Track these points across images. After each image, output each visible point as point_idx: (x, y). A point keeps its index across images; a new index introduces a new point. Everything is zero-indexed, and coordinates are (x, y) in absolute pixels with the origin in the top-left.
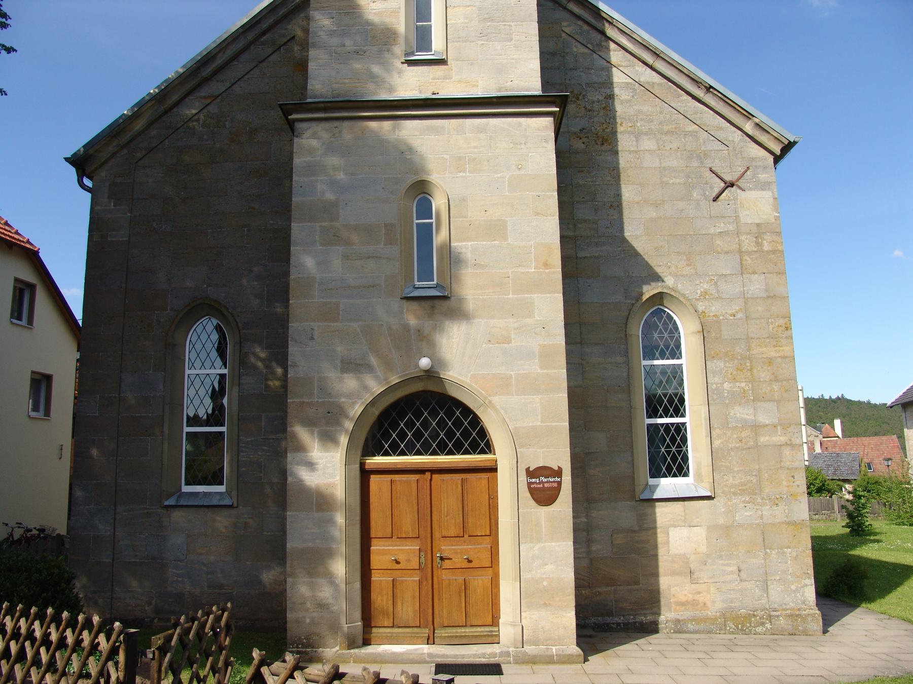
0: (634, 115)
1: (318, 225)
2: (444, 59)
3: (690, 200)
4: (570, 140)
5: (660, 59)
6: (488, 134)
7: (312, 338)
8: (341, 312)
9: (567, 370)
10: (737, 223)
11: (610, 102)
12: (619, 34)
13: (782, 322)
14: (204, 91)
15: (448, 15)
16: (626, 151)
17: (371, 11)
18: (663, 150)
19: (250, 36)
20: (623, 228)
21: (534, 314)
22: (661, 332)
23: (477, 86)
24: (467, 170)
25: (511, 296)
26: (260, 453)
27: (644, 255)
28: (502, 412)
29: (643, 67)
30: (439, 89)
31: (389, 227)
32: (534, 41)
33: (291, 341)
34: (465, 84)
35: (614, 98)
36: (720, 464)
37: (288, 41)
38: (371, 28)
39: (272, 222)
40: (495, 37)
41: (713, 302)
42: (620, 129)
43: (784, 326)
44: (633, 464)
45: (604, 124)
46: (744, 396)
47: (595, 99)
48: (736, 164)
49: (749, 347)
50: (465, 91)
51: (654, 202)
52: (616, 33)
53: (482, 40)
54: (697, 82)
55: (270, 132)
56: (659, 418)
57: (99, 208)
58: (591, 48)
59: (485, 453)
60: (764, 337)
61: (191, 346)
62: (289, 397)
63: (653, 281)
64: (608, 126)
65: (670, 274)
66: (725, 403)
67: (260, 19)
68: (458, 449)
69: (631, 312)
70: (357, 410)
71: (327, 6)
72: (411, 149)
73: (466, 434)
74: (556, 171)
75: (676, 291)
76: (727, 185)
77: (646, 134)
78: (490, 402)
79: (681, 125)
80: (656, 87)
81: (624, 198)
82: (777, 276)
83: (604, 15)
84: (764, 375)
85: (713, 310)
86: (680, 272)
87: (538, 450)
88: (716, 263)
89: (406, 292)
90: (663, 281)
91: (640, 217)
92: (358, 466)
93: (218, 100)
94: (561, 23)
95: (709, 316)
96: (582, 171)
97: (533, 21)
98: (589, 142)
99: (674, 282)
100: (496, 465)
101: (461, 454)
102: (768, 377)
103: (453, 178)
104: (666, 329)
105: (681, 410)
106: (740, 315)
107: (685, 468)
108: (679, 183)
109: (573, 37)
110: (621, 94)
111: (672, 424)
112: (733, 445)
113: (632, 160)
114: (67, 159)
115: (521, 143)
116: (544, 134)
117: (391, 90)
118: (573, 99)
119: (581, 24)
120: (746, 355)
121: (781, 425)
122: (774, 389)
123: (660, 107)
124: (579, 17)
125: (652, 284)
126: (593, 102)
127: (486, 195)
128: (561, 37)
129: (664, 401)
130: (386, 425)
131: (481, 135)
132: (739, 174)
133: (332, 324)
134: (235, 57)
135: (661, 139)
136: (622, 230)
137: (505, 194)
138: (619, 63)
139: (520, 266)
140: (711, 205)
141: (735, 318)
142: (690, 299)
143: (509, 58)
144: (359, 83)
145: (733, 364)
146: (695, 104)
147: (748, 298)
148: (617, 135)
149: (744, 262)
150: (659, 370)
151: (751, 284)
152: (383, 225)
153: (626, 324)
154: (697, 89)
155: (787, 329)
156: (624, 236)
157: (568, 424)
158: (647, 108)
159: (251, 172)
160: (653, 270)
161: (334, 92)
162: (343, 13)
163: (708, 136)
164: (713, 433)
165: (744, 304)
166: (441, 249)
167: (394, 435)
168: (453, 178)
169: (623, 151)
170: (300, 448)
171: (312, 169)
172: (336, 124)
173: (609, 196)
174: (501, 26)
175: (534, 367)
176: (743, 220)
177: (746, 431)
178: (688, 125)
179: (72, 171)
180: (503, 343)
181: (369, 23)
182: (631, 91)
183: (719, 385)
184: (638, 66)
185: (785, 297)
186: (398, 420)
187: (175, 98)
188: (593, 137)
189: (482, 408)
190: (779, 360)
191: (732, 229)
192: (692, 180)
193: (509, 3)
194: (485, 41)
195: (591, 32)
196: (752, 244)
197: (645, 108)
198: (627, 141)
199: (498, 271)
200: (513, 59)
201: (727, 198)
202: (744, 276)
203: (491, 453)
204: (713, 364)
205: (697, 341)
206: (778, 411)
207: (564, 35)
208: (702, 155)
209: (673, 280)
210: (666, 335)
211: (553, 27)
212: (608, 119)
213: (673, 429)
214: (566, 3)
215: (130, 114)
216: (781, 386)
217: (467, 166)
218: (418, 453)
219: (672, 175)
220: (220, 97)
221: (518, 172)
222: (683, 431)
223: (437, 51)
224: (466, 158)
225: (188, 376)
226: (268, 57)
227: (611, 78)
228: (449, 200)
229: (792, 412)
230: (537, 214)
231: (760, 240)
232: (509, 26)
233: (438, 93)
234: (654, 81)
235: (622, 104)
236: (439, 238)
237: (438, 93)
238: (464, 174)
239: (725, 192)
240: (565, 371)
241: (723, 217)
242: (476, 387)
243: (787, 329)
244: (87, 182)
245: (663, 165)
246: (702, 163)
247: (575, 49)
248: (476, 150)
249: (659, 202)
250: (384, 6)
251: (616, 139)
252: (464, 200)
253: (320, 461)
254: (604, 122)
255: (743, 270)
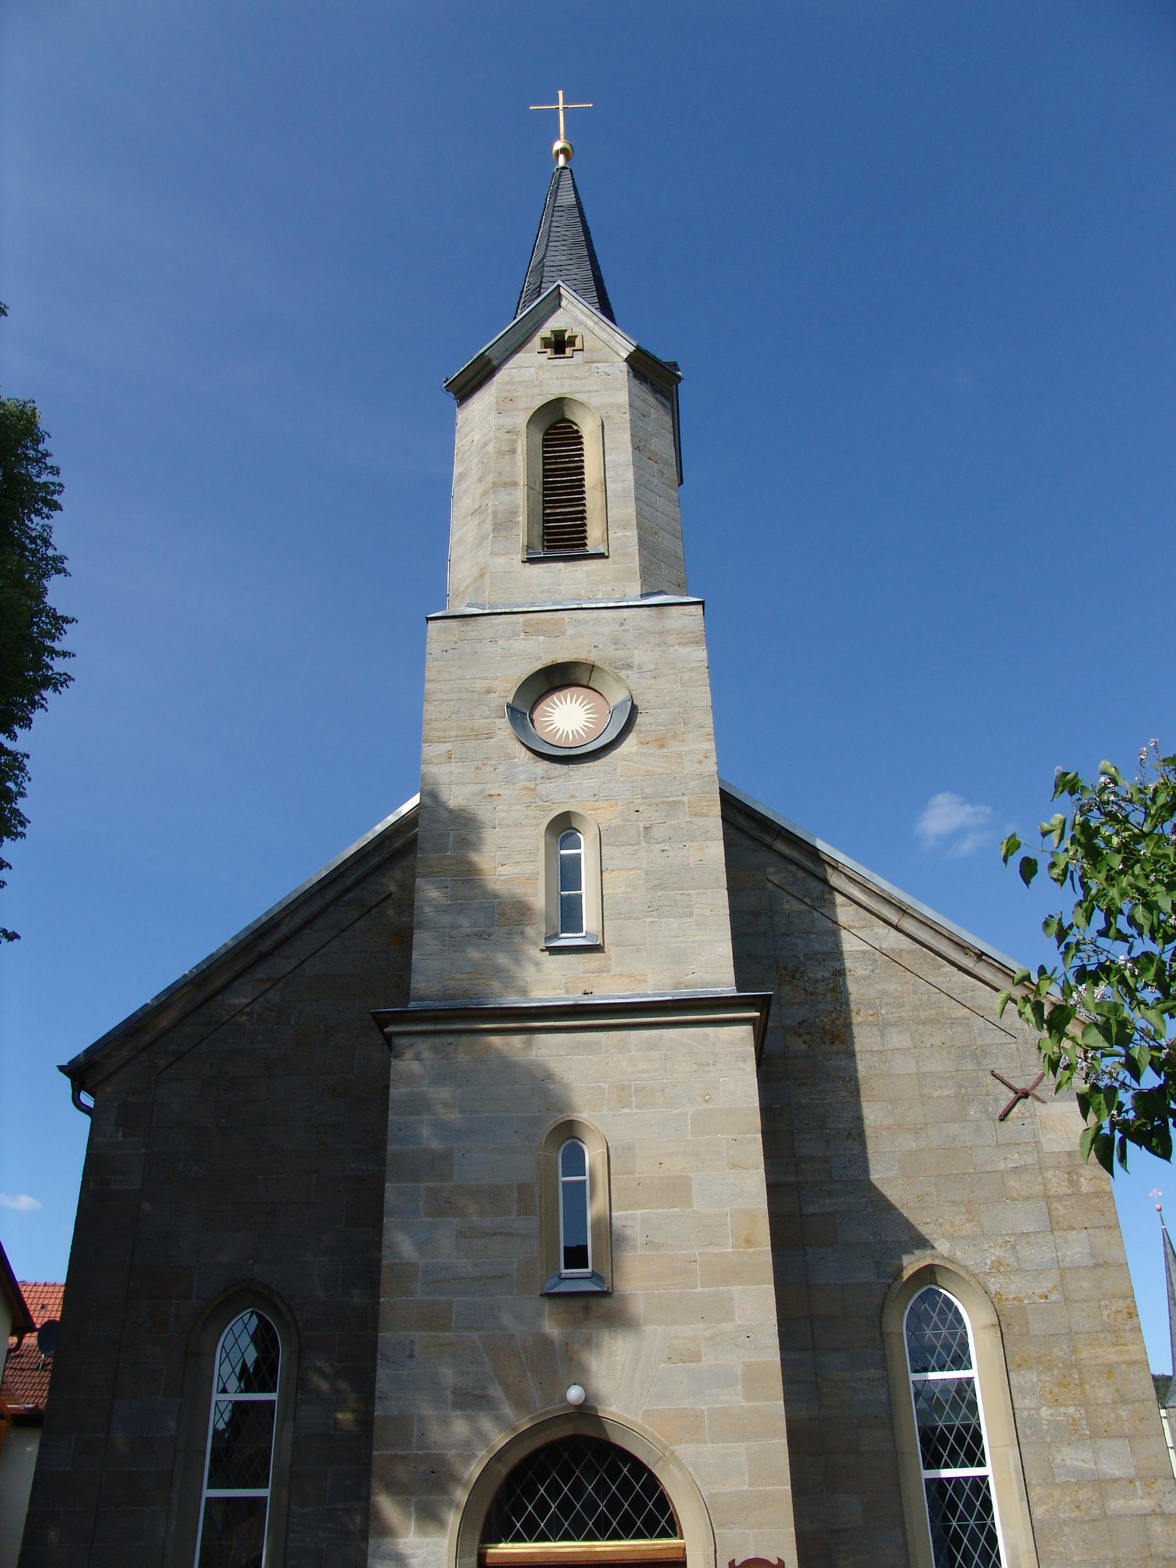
0: (877, 998)
1: (423, 1185)
2: (600, 944)
3: (966, 1120)
4: (784, 1038)
5: (908, 916)
6: (662, 1052)
7: (411, 1356)
8: (454, 1316)
9: (784, 1401)
10: (1038, 1153)
11: (841, 980)
12: (848, 882)
13: (1121, 1304)
14: (262, 972)
15: (603, 882)
16: (867, 1051)
17: (498, 877)
18: (921, 1048)
19: (330, 894)
20: (868, 1167)
21: (734, 1315)
22: (936, 1327)
23: (646, 982)
24: (634, 1104)
25: (699, 1289)
26: (321, 1534)
27: (902, 1208)
28: (691, 1469)
29: (885, 928)
30: (593, 987)
31: (524, 1190)
32: (723, 916)
33: (381, 1359)
34: (629, 978)
35: (845, 974)
36: (1048, 1548)
37: (382, 901)
38: (499, 902)
39: (353, 1166)
40: (670, 910)
41: (1011, 1277)
42: (856, 1019)
43: (1125, 1312)
44: (907, 1550)
45: (833, 1012)
46: (1075, 1430)
47: (819, 976)
48: (1029, 1063)
49: (1073, 1348)
50: (628, 989)
51: (912, 1126)
52: (844, 881)
53: (650, 916)
54: (963, 947)
55: (354, 1031)
56: (943, 1468)
57: (100, 1139)
58: (810, 904)
59: (668, 1536)
60: (1096, 1329)
61: (224, 1355)
62: (375, 1447)
63: (918, 1248)
64: (840, 1016)
65: (943, 1235)
66: (1046, 1442)
67: (344, 871)
68: (627, 1530)
69: (888, 1296)
70: (474, 1471)
71: (440, 870)
72: (549, 1076)
73: (638, 1505)
74: (758, 1103)
75: (954, 1263)
76: (1019, 1095)
77: (895, 1025)
78: (672, 1453)
79: (945, 1009)
80: (905, 956)
81: (866, 1122)
82: (1106, 1231)
83: (825, 858)
84: (1102, 1393)
85: (1012, 1290)
86: (958, 1232)
87: (746, 1531)
88: (1012, 1215)
89: (548, 1285)
90: (933, 1247)
91: (893, 1149)
92: (474, 1559)
93: (281, 984)
94: (765, 870)
95: (1007, 1300)
96: (804, 1084)
97: (720, 888)
98: (812, 1040)
99: (950, 1248)
100: (685, 1556)
101: (631, 1538)
102: (1109, 1397)
103: (614, 1116)
104: (944, 1321)
105: (977, 1454)
106: (1054, 1297)
107: (994, 1556)
108: (947, 1096)
109: (783, 889)
110: (855, 969)
111: (966, 1479)
112: (1067, 1515)
113: (877, 1064)
114: (61, 1068)
115: (708, 1064)
116: (739, 1049)
117: (524, 992)
118: (787, 978)
119: (794, 869)
120: (1072, 1362)
121: (1141, 1479)
122: (1121, 1416)
123: (913, 984)
124: (790, 861)
125: (916, 1252)
126: (816, 981)
127: (661, 1140)
128: (766, 889)
129: (949, 1439)
130: (518, 1491)
131: (653, 1054)
132: (1035, 1078)
133: (441, 1334)
134: (308, 923)
135: (916, 1031)
136: (866, 1171)
137: (687, 1138)
138: (851, 923)
139: (711, 1243)
140: (997, 1127)
141: (1048, 1301)
142: (975, 1274)
143: (689, 940)
144: (482, 978)
145: (1052, 1376)
146: (962, 978)
147: (1064, 1269)
148: (852, 1029)
149: (1054, 1213)
150: (938, 1389)
151: (1067, 1247)
152: (515, 1186)
153: (881, 1317)
154: (964, 956)
155: (1130, 1315)
156: (869, 1179)
157: (790, 1488)
158: (894, 986)
159: (324, 1090)
160: (916, 1230)
161: (448, 992)
162: (460, 880)
163: (986, 1024)
164: (1031, 1494)
165: (1059, 1279)
166: (597, 1223)
167: (530, 1508)
168: (614, 1116)
169: (863, 1052)
170: (386, 1531)
171: (418, 1105)
172: (450, 1039)
173: (846, 1119)
174: (677, 895)
175: (735, 1398)
176: (1047, 1147)
177: (1085, 1490)
178: (955, 1009)
179: (66, 1082)
180: (689, 1362)
181: (495, 896)
182: (870, 962)
183: (1032, 1412)
184: (878, 926)
185: (1121, 1265)
186: (536, 1482)
187: (220, 981)
188: (819, 1032)
189: (660, 1464)
190: (1124, 1367)
191: (1032, 1162)
192: (966, 1089)
193: (687, 863)
194: (654, 917)
195: (808, 880)
196: (1063, 1184)
197: (891, 987)
198: (867, 1036)
199: (681, 1252)
200: (694, 942)
201: (1020, 1115)
202: (1056, 1235)
203: (676, 1536)
204: (1021, 1377)
205: (991, 1339)
206: (1133, 1454)
207: (770, 885)
208: (978, 1051)
209: (948, 1245)
210: (944, 1331)
211: (754, 876)
212: (838, 1005)
213: (967, 1488)
214: (771, 841)
215: (155, 1005)
216: (1133, 1412)
217: (633, 1098)
218: (567, 1537)
219: (937, 1084)
220: (283, 980)
221: (706, 1106)
222: (984, 1490)
223: (590, 933)
224: (631, 1088)
225: (217, 1404)
226: (354, 922)
227: (840, 945)
228: (608, 1149)
229: (1155, 1456)
230: (734, 1166)
231: (1075, 1177)
232: (688, 895)
233: (591, 993)
234: (903, 947)
235: (857, 982)
236: (594, 1209)
237: (591, 993)
238: (629, 1111)
239: (1017, 1106)
240: (783, 1403)
241: (1016, 1144)
242: (651, 1429)
243: (1130, 1315)
244: (87, 1099)
245: (923, 1070)
246: (979, 1063)
247: (787, 906)
248: (646, 1075)
249: (919, 1126)
250: (517, 870)
251: (852, 1033)
252: (630, 1148)
253: (417, 1551)
254: (832, 1009)
255: (1053, 1225)
